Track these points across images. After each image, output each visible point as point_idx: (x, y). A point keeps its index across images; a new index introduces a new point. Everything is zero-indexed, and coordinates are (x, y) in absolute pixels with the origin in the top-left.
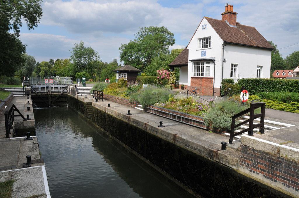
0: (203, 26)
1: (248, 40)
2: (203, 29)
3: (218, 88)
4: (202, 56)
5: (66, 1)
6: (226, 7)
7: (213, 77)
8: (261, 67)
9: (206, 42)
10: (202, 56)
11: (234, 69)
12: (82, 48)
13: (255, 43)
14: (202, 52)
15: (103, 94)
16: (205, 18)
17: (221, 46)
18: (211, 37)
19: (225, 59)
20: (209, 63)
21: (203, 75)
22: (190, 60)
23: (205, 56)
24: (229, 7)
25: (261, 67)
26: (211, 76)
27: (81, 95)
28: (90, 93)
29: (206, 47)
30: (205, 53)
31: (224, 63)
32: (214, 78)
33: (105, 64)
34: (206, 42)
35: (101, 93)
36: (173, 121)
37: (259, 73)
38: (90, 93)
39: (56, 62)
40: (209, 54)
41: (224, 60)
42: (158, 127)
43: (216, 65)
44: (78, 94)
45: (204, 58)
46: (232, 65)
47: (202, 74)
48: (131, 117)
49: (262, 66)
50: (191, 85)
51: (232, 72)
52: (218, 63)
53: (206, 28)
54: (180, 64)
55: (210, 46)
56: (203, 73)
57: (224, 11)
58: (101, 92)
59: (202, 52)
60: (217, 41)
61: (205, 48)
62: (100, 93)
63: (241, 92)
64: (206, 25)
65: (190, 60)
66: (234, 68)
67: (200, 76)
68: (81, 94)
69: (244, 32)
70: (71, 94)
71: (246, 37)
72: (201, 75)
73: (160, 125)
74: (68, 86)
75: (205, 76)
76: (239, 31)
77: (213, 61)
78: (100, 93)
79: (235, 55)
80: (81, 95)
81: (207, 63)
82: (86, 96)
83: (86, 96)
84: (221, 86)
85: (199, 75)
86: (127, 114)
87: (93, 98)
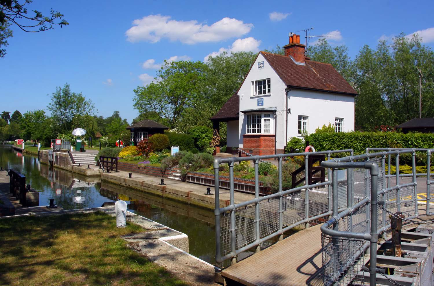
0: (259, 64)
1: (321, 82)
3: (282, 150)
6: (291, 38)
7: (274, 134)
8: (341, 120)
9: (262, 85)
10: (258, 105)
11: (303, 122)
12: (66, 93)
13: (331, 86)
14: (258, 99)
15: (117, 163)
18: (270, 78)
19: (289, 110)
20: (269, 116)
21: (260, 132)
22: (241, 112)
23: (263, 105)
24: (295, 37)
25: (341, 119)
26: (272, 133)
27: (79, 165)
28: (94, 160)
30: (263, 101)
32: (275, 136)
33: (99, 119)
35: (114, 160)
37: (339, 128)
38: (94, 160)
39: (13, 115)
40: (268, 104)
41: (289, 111)
42: (205, 196)
43: (277, 142)
44: (74, 164)
46: (300, 117)
47: (259, 131)
48: (166, 187)
49: (343, 118)
50: (244, 147)
51: (300, 127)
52: (281, 116)
53: (263, 66)
54: (228, 117)
56: (260, 130)
57: (287, 43)
58: (114, 158)
59: (258, 99)
60: (278, 85)
62: (112, 160)
64: (263, 63)
65: (241, 112)
66: (303, 121)
67: (257, 134)
68: (79, 164)
69: (316, 71)
70: (60, 165)
71: (318, 78)
73: (161, 183)
74: (54, 153)
75: (263, 133)
76: (309, 70)
78: (112, 160)
79: (301, 104)
80: (79, 165)
81: (265, 116)
82: (89, 166)
83: (89, 166)
84: (285, 147)
85: (255, 132)
86: (159, 184)
87: (100, 168)
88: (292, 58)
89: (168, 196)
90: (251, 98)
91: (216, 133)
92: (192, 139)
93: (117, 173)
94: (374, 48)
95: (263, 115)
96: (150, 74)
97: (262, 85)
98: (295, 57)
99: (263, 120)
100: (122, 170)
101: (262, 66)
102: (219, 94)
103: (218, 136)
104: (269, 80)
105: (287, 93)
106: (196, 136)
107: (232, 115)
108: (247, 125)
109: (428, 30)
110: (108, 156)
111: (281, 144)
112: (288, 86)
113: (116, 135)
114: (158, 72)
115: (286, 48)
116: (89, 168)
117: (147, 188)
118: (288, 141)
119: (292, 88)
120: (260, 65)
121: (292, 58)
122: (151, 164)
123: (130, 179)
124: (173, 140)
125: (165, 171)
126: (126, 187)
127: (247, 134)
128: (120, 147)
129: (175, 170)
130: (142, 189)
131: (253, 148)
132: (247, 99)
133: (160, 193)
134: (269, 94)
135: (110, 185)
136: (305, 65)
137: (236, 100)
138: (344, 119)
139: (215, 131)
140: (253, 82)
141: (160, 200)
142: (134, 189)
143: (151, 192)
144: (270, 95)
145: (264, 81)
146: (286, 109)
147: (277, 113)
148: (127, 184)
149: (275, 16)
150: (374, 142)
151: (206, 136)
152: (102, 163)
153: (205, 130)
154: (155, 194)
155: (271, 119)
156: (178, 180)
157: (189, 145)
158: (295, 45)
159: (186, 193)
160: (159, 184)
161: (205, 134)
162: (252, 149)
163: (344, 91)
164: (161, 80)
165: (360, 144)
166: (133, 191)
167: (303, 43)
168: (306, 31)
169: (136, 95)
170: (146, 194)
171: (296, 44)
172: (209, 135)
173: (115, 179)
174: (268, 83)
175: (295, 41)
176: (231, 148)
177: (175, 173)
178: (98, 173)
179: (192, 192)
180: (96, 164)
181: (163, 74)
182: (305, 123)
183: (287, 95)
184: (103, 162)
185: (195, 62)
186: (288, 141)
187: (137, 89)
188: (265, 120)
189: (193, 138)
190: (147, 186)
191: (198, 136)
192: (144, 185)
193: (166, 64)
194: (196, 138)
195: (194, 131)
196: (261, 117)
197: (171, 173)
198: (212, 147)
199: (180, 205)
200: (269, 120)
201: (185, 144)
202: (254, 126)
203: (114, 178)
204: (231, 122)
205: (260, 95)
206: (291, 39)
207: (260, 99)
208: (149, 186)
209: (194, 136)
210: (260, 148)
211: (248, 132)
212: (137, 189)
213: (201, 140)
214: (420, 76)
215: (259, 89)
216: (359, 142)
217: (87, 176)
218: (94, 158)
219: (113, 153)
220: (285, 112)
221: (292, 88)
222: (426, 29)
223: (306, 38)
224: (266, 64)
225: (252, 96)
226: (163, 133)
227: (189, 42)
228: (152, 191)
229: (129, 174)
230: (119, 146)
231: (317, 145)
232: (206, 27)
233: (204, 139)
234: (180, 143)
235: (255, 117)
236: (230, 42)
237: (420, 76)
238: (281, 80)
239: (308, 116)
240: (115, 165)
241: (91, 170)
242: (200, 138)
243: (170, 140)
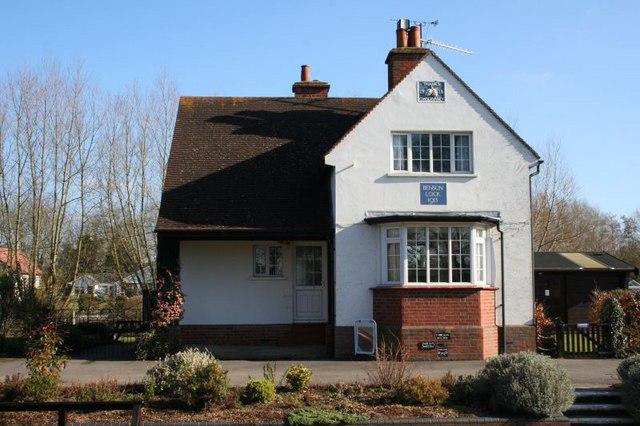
10: (424, 201)
18: (471, 133)
21: (467, 278)
40: (461, 198)
59: (422, 185)
72: (433, 279)
131: (452, 328)
211: (412, 279)
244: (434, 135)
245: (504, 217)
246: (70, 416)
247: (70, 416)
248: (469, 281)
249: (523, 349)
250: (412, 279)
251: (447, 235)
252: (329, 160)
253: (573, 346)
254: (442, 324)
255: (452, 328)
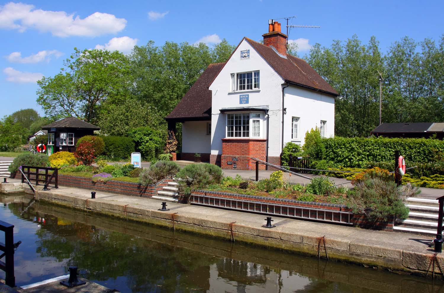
0: (242, 52)
2: (242, 57)
3: (276, 158)
4: (241, 103)
5: (120, 37)
6: (271, 25)
10: (241, 103)
11: (295, 125)
16: (247, 40)
17: (281, 88)
18: (259, 71)
21: (248, 135)
23: (248, 103)
24: (276, 25)
26: (263, 137)
29: (248, 88)
31: (285, 115)
32: (267, 141)
34: (247, 80)
36: (172, 203)
40: (255, 101)
45: (245, 106)
49: (326, 121)
52: (275, 117)
53: (249, 56)
55: (255, 87)
57: (267, 32)
59: (240, 96)
60: (271, 80)
61: (246, 90)
63: (130, 155)
64: (248, 51)
67: (242, 138)
71: (303, 74)
72: (244, 136)
73: (163, 208)
75: (251, 137)
77: (264, 112)
85: (240, 136)
86: (2, 183)
87: (23, 182)
88: (274, 49)
89: (184, 229)
90: (229, 94)
91: (173, 136)
92: (132, 143)
93: (57, 190)
94: (364, 42)
95: (251, 116)
96: (53, 64)
97: (247, 80)
98: (277, 48)
99: (251, 121)
100: (63, 185)
101: (246, 55)
102: (149, 90)
103: (174, 140)
104: (257, 73)
105: (283, 89)
106: (138, 139)
107: (197, 113)
108: (227, 127)
109: (298, 39)
110: (29, 165)
111: (275, 151)
112: (286, 81)
113: (7, 137)
114: (66, 62)
115: (265, 37)
116: (6, 182)
117: (135, 215)
118: (285, 145)
119: (289, 84)
120: (244, 55)
121: (274, 49)
122: (114, 177)
123: (93, 200)
124: (110, 143)
125: (146, 188)
126: (89, 212)
127: (227, 138)
128: (42, 152)
129: (160, 187)
130: (124, 215)
131: (238, 156)
132: (223, 94)
133: (167, 223)
134: (257, 89)
135: (54, 208)
136: (286, 58)
137: (207, 97)
138: (327, 122)
139: (172, 134)
140: (233, 75)
141: (168, 234)
142: (107, 216)
143: (144, 220)
144: (259, 91)
145: (249, 74)
146: (282, 109)
147: (269, 113)
148: (91, 208)
149: (153, 15)
150: (408, 149)
151: (151, 140)
152: (27, 175)
153: (149, 132)
154: (153, 224)
155: (261, 121)
156: (172, 202)
157: (129, 150)
158: (278, 34)
159: (225, 225)
160: (159, 210)
161: (148, 136)
162: (237, 156)
163: (329, 91)
164: (69, 70)
165: (389, 152)
166: (104, 218)
167: (283, 32)
168: (287, 19)
169: (40, 88)
170: (134, 224)
171: (280, 33)
172: (154, 138)
173: (65, 200)
174: (255, 76)
175: (276, 30)
176: (194, 154)
177: (160, 191)
178: (21, 190)
179: (236, 224)
180: (9, 176)
181: (73, 64)
182: (296, 126)
183: (283, 91)
184: (29, 174)
185: (112, 52)
186: (285, 145)
187: (42, 79)
188: (254, 121)
189: (134, 141)
190: (136, 212)
191: (141, 138)
192: (128, 210)
193: (76, 53)
194: (138, 141)
195: (135, 133)
196: (248, 117)
197: (156, 191)
198: (167, 153)
199: (212, 242)
200: (259, 121)
201: (124, 149)
202: (238, 128)
203: (57, 197)
204: (186, 122)
205: (243, 91)
206: (271, 27)
207: (243, 95)
208: (142, 212)
209: (136, 139)
210: (249, 155)
211: (229, 136)
212: (113, 216)
213: (144, 143)
214: (380, 79)
215: (241, 83)
216: (389, 150)
217: (4, 194)
218: (8, 167)
219: (36, 161)
220: (281, 112)
221: (289, 84)
222: (297, 39)
223: (287, 27)
224: (253, 53)
225: (231, 91)
226: (92, 134)
227: (60, 35)
228: (147, 220)
229: (92, 193)
230: (41, 151)
231: (330, 153)
232: (78, 20)
233: (148, 143)
234: (119, 147)
235: (238, 119)
236: (107, 38)
237: (380, 79)
238: (276, 74)
239: (299, 118)
240: (54, 179)
241: (9, 185)
242: (143, 142)
243: (106, 143)
244: (247, 73)
245: (270, 108)
246: (30, 169)
247: (30, 169)
248: (249, 136)
249: (405, 161)
250: (229, 136)
251: (233, 117)
252: (210, 89)
253: (167, 196)
254: (236, 154)
255: (238, 156)
